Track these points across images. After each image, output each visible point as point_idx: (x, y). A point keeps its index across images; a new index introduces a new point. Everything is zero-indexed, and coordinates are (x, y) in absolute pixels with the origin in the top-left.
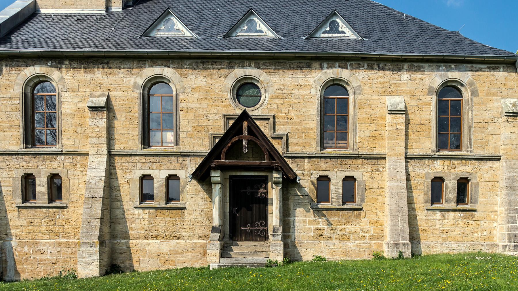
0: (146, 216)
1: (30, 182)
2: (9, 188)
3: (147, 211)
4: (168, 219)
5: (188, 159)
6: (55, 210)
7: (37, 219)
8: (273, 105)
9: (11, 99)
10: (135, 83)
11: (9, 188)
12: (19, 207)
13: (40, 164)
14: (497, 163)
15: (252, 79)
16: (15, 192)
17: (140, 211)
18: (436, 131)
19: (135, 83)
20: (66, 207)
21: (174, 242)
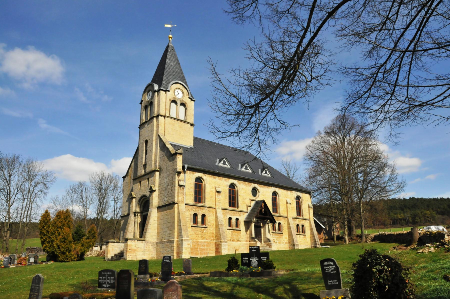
0: (230, 233)
1: (387, 260)
2: (189, 219)
3: (231, 230)
4: (236, 234)
5: (241, 213)
6: (204, 228)
7: (198, 232)
8: (354, 213)
9: (190, 184)
10: (227, 184)
11: (189, 219)
12: (192, 226)
13: (199, 210)
14: (223, 207)
15: (204, 181)
16: (191, 220)
17: (229, 230)
18: (204, 195)
19: (227, 184)
20: (206, 228)
21: (239, 243)
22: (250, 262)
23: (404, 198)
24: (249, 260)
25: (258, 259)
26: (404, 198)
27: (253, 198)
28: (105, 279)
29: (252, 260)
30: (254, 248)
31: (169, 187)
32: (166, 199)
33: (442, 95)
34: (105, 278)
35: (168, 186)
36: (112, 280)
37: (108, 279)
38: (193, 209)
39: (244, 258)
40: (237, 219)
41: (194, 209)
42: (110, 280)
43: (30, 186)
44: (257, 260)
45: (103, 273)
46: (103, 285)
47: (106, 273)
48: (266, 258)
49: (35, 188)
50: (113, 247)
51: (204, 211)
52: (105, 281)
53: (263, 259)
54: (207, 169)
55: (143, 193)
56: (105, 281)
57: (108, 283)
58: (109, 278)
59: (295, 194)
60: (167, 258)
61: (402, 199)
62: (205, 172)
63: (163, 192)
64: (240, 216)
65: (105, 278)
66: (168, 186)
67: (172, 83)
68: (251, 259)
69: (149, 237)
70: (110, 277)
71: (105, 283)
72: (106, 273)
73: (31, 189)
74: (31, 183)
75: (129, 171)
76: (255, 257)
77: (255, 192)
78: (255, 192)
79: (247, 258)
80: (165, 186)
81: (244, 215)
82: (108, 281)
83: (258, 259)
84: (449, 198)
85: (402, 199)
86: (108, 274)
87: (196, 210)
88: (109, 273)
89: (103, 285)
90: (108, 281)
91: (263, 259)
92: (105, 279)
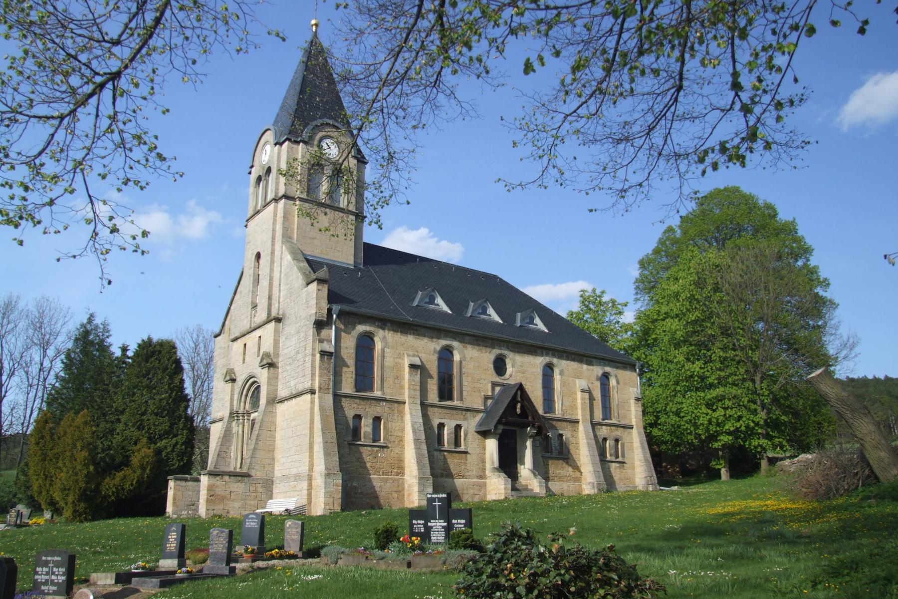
4: (456, 461)
6: (377, 449)
10: (435, 349)
13: (367, 407)
22: (428, 529)
23: (886, 377)
24: (425, 525)
25: (445, 524)
26: (886, 377)
27: (498, 379)
28: (47, 573)
29: (432, 527)
30: (438, 498)
31: (300, 356)
32: (292, 383)
33: (624, 30)
34: (47, 569)
35: (298, 352)
36: (61, 575)
37: (53, 573)
38: (353, 406)
39: (414, 522)
40: (458, 428)
41: (355, 406)
42: (57, 575)
43: (44, 358)
44: (443, 527)
45: (44, 558)
46: (43, 588)
47: (49, 558)
48: (463, 521)
49: (53, 363)
50: (183, 489)
51: (379, 409)
52: (47, 577)
53: (457, 524)
54: (386, 315)
55: (249, 371)
56: (47, 577)
57: (53, 583)
58: (55, 569)
59: (598, 370)
60: (252, 518)
61: (882, 378)
62: (384, 322)
63: (288, 368)
64: (465, 419)
65: (47, 569)
66: (298, 352)
67: (319, 122)
68: (429, 524)
69: (256, 468)
70: (57, 567)
71: (46, 583)
72: (49, 558)
73: (47, 364)
74: (45, 352)
75: (227, 323)
76: (440, 519)
77: (500, 366)
78: (500, 366)
79: (422, 522)
80: (293, 353)
81: (474, 417)
82: (53, 577)
83: (445, 524)
84: (894, 375)
85: (882, 378)
86: (53, 562)
87: (360, 407)
88: (56, 558)
89: (43, 588)
90: (53, 577)
91: (457, 524)
92: (47, 573)
